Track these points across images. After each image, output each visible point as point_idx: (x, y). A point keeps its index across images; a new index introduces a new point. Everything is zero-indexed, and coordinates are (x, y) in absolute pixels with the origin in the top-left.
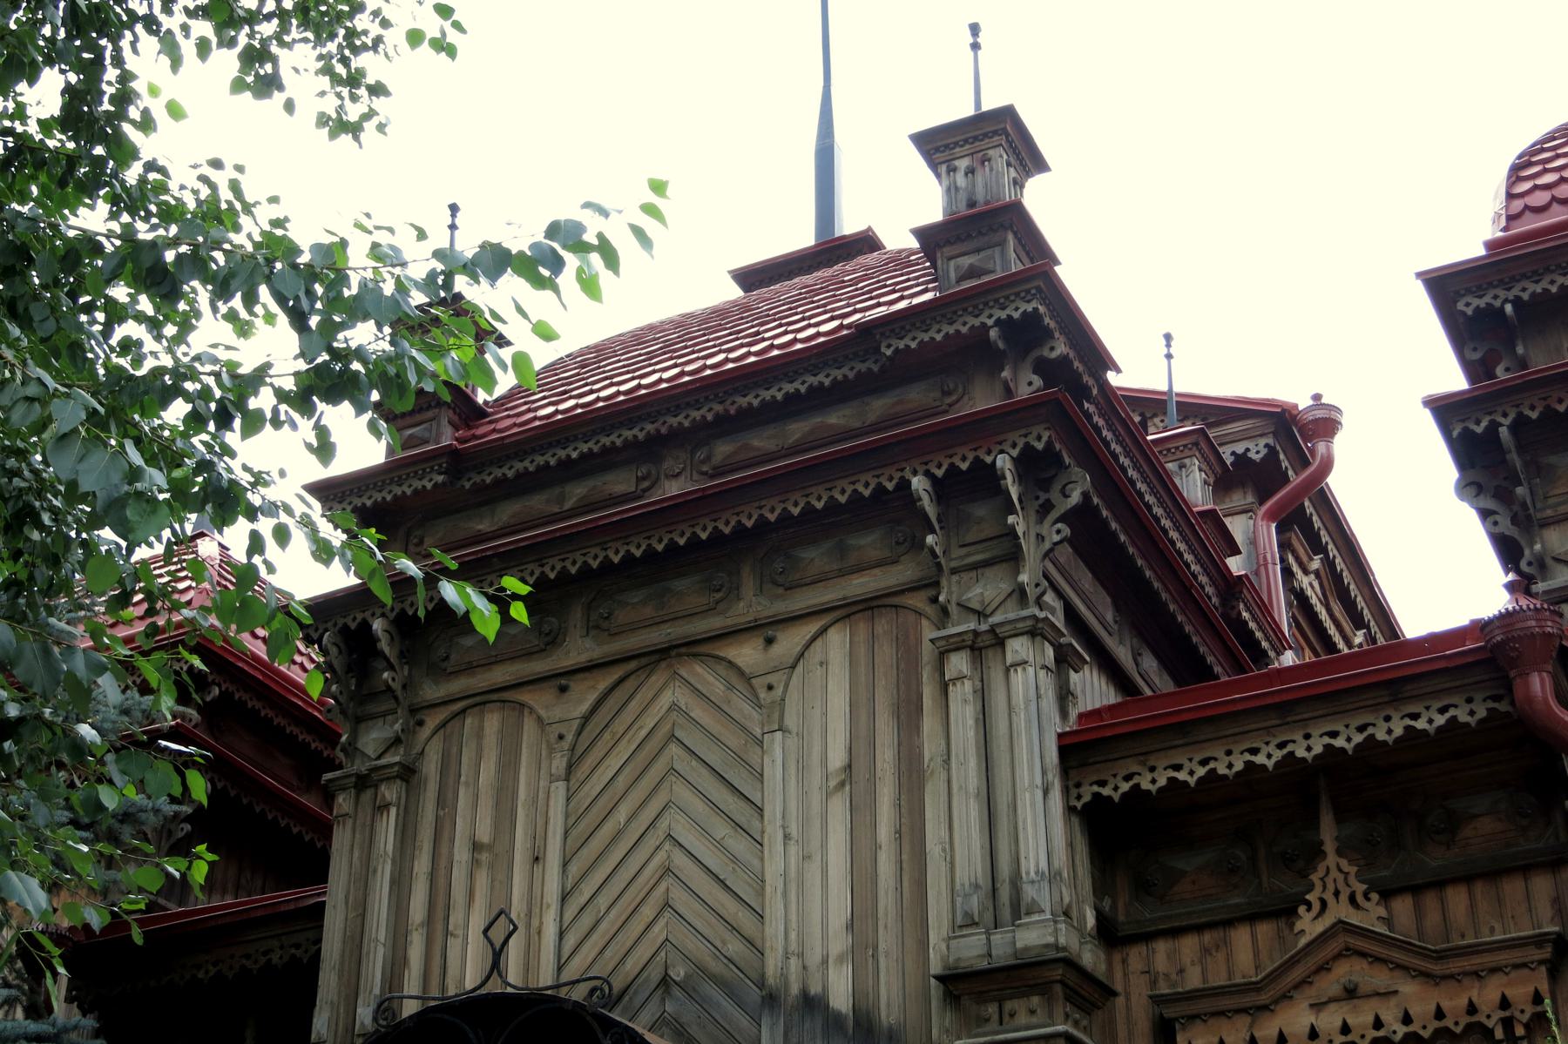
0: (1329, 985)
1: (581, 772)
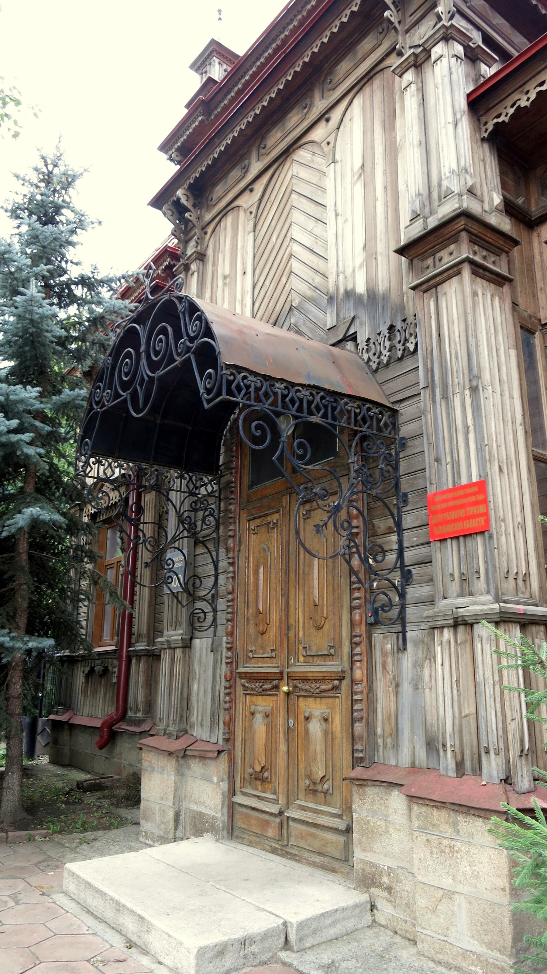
1: (259, 227)
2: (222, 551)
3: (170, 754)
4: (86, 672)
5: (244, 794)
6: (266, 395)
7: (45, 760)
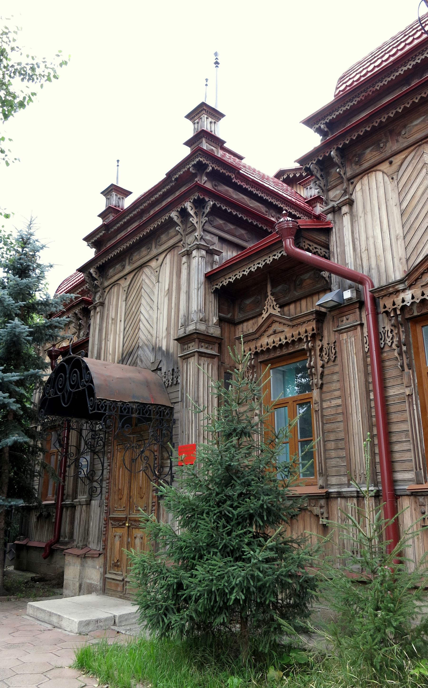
0: (271, 331)
1: (128, 299)
2: (106, 458)
3: (78, 556)
4: (38, 515)
5: (110, 573)
6: (114, 408)
7: (11, 568)
